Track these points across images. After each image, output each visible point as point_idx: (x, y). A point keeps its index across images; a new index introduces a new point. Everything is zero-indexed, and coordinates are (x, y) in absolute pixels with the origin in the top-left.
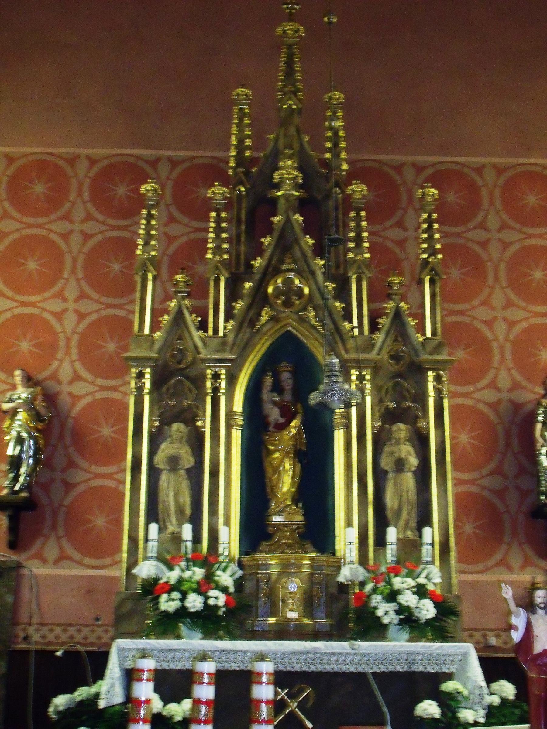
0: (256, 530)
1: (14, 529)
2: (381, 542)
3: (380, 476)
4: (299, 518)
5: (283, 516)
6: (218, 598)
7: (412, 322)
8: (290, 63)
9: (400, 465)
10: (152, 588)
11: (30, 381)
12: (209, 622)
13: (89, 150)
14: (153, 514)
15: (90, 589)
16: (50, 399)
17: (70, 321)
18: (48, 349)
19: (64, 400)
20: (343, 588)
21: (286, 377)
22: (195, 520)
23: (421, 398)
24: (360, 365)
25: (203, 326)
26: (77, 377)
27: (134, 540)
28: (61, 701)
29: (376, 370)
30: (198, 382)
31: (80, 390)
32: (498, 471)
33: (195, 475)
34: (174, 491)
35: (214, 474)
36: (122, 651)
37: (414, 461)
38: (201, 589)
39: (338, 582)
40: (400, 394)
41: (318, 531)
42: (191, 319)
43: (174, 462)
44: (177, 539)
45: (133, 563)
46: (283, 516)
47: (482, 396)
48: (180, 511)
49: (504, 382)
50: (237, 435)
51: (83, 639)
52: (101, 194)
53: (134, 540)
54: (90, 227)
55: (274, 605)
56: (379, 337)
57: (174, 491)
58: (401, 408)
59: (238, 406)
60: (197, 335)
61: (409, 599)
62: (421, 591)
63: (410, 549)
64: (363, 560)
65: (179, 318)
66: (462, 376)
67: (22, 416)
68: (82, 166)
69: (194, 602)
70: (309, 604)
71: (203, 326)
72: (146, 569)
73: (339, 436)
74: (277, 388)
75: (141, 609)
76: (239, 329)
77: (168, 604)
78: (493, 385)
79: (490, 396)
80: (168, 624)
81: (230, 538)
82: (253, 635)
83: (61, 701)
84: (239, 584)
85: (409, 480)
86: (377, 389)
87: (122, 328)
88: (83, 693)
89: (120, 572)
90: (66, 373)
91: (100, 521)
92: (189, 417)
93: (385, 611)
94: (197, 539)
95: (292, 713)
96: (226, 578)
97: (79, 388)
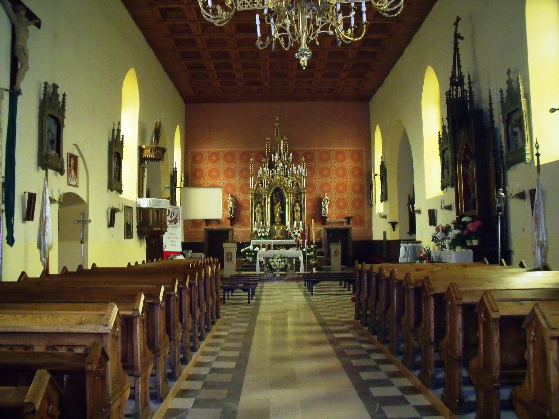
0: (273, 222)
1: (231, 222)
2: (294, 224)
3: (294, 212)
4: (280, 220)
5: (278, 219)
6: (267, 234)
7: (300, 184)
8: (277, 132)
9: (297, 211)
10: (256, 232)
11: (232, 196)
12: (265, 237)
13: (239, 149)
14: (255, 220)
15: (245, 232)
16: (235, 199)
17: (237, 184)
18: (234, 190)
19: (238, 199)
20: (287, 231)
21: (277, 195)
22: (262, 221)
23: (301, 199)
24: (290, 193)
25: (262, 186)
26: (240, 195)
27: (252, 224)
28: (243, 250)
29: (293, 193)
30: (262, 196)
31: (241, 197)
32: (315, 210)
33: (262, 213)
34: (258, 216)
35: (265, 213)
36: (254, 242)
37: (299, 210)
38: (264, 232)
39: (431, 199)
40: (297, 198)
41: (283, 222)
42: (260, 185)
43: (258, 211)
44: (260, 224)
45: (252, 228)
46: (278, 219)
47: (313, 196)
48: (260, 219)
49: (318, 194)
50: (269, 205)
51: (247, 240)
52: (241, 158)
53: (252, 224)
54: (240, 165)
55: (275, 234)
56: (294, 188)
57: (258, 216)
58: (298, 200)
59: (269, 201)
60: (261, 188)
61: (296, 233)
62: (299, 232)
63: (298, 225)
64: (291, 227)
65: (258, 185)
66: (309, 192)
67: (231, 203)
68: (237, 153)
69: (263, 234)
70: (281, 234)
71: (262, 186)
72: (255, 229)
73: (287, 205)
74: (276, 196)
75: (254, 235)
76: (269, 186)
77: (259, 235)
78: (316, 194)
79: (315, 196)
80: (259, 238)
81: (268, 224)
82: (274, 239)
83: (243, 250)
84: (270, 231)
85: (299, 213)
86: (293, 197)
87: (247, 185)
88: (246, 248)
89: (250, 229)
90: (238, 194)
91: (246, 221)
92: (260, 203)
93: (292, 235)
94: (263, 224)
95: (328, 30)
96: (268, 231)
97: (240, 197)
